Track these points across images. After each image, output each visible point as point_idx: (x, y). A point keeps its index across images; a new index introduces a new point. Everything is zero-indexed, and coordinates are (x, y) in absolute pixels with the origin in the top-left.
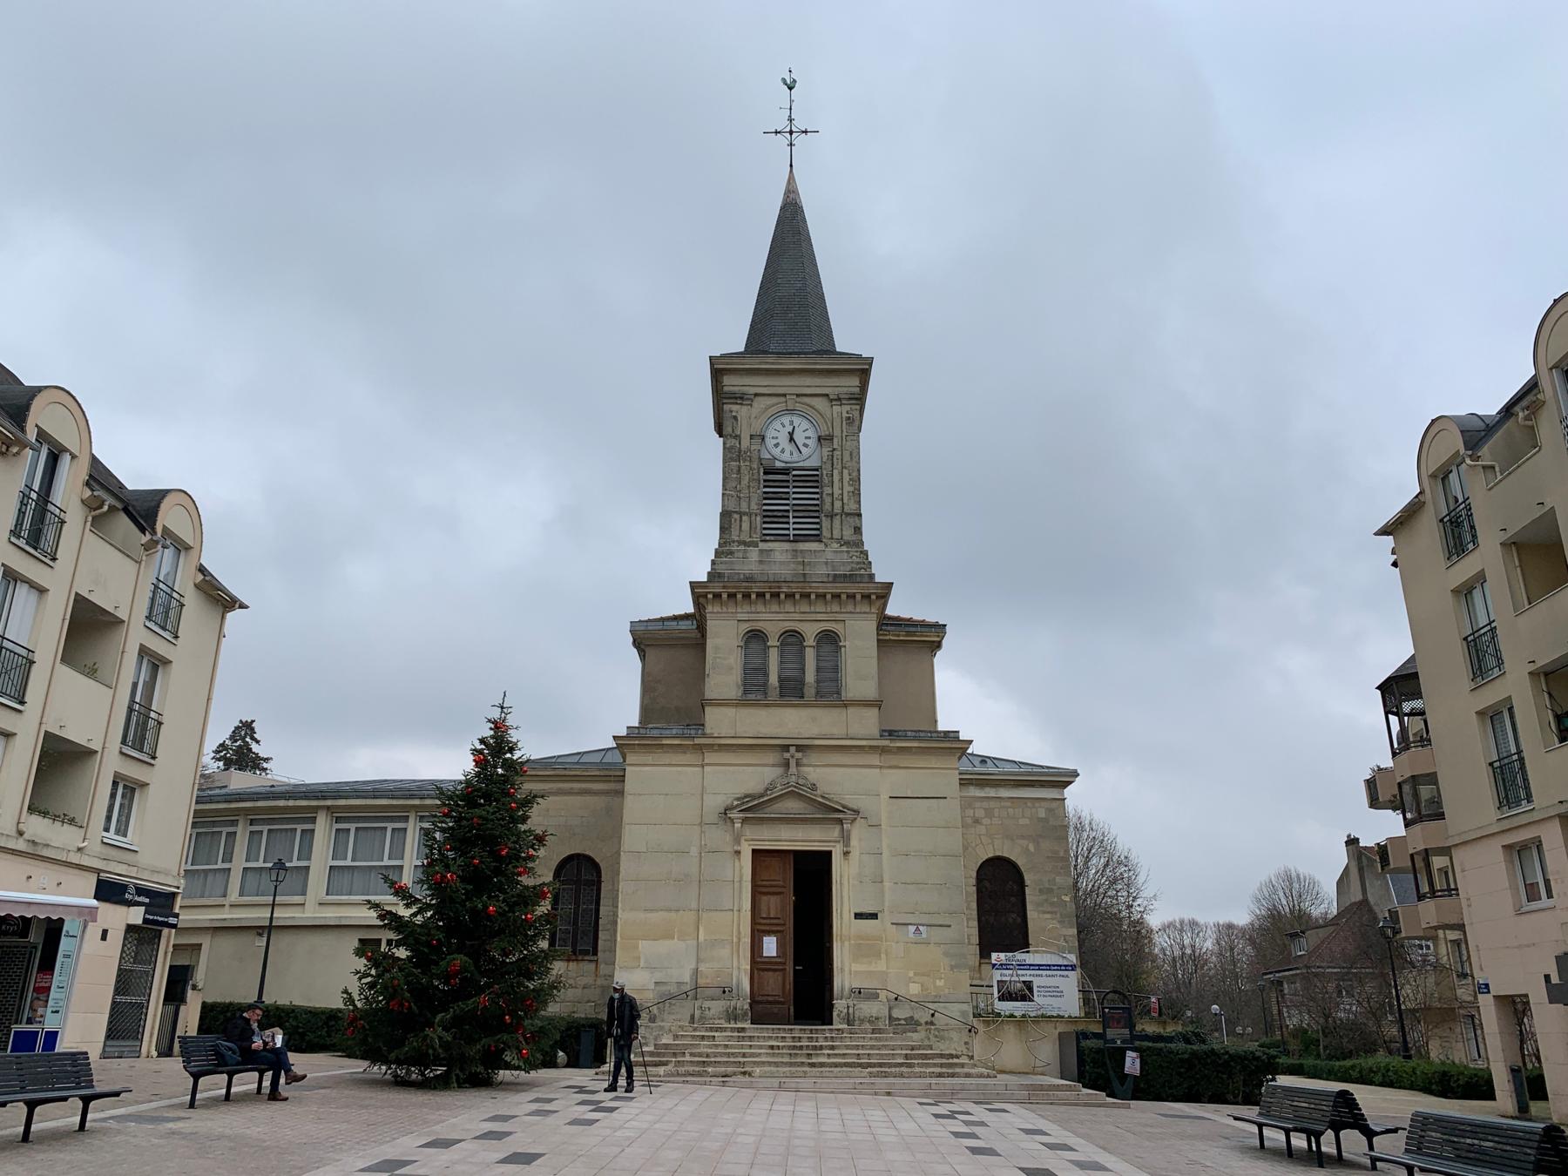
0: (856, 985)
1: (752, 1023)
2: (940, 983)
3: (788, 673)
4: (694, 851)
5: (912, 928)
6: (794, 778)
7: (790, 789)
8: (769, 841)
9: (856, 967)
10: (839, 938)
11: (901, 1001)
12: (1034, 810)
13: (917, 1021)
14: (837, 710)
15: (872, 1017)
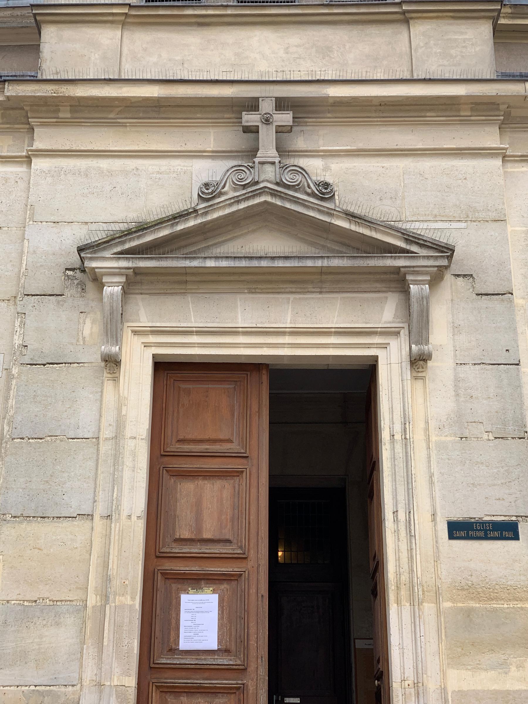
7: (262, 199)
10: (404, 593)
14: (388, 31)
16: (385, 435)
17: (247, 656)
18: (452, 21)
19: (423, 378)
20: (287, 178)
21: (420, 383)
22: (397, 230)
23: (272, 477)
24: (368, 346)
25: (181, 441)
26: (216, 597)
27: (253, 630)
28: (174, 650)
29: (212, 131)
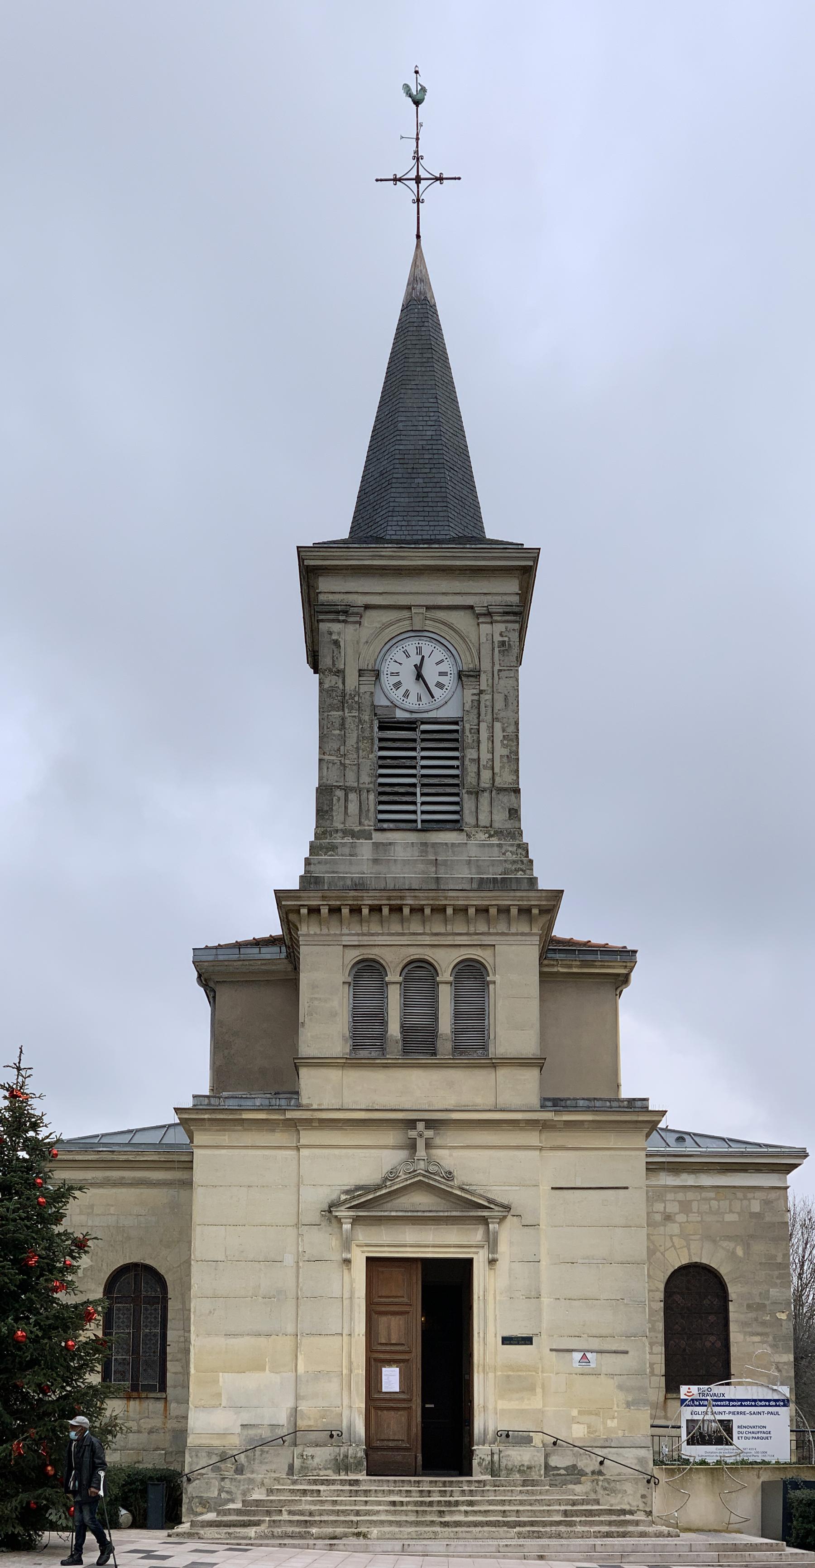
0: (504, 1426)
1: (368, 1475)
2: (611, 1424)
3: (415, 1021)
5: (577, 1356)
6: (422, 1165)
9: (502, 1405)
10: (481, 1368)
12: (745, 1202)
13: (582, 1470)
15: (523, 1465)
16: (475, 1297)
17: (412, 1395)
18: (519, 1068)
19: (494, 1269)
20: (432, 1168)
21: (493, 1271)
22: (484, 1197)
23: (422, 1282)
24: (469, 1253)
25: (380, 1297)
26: (398, 1369)
27: (414, 1383)
28: (380, 1392)
29: (392, 1132)
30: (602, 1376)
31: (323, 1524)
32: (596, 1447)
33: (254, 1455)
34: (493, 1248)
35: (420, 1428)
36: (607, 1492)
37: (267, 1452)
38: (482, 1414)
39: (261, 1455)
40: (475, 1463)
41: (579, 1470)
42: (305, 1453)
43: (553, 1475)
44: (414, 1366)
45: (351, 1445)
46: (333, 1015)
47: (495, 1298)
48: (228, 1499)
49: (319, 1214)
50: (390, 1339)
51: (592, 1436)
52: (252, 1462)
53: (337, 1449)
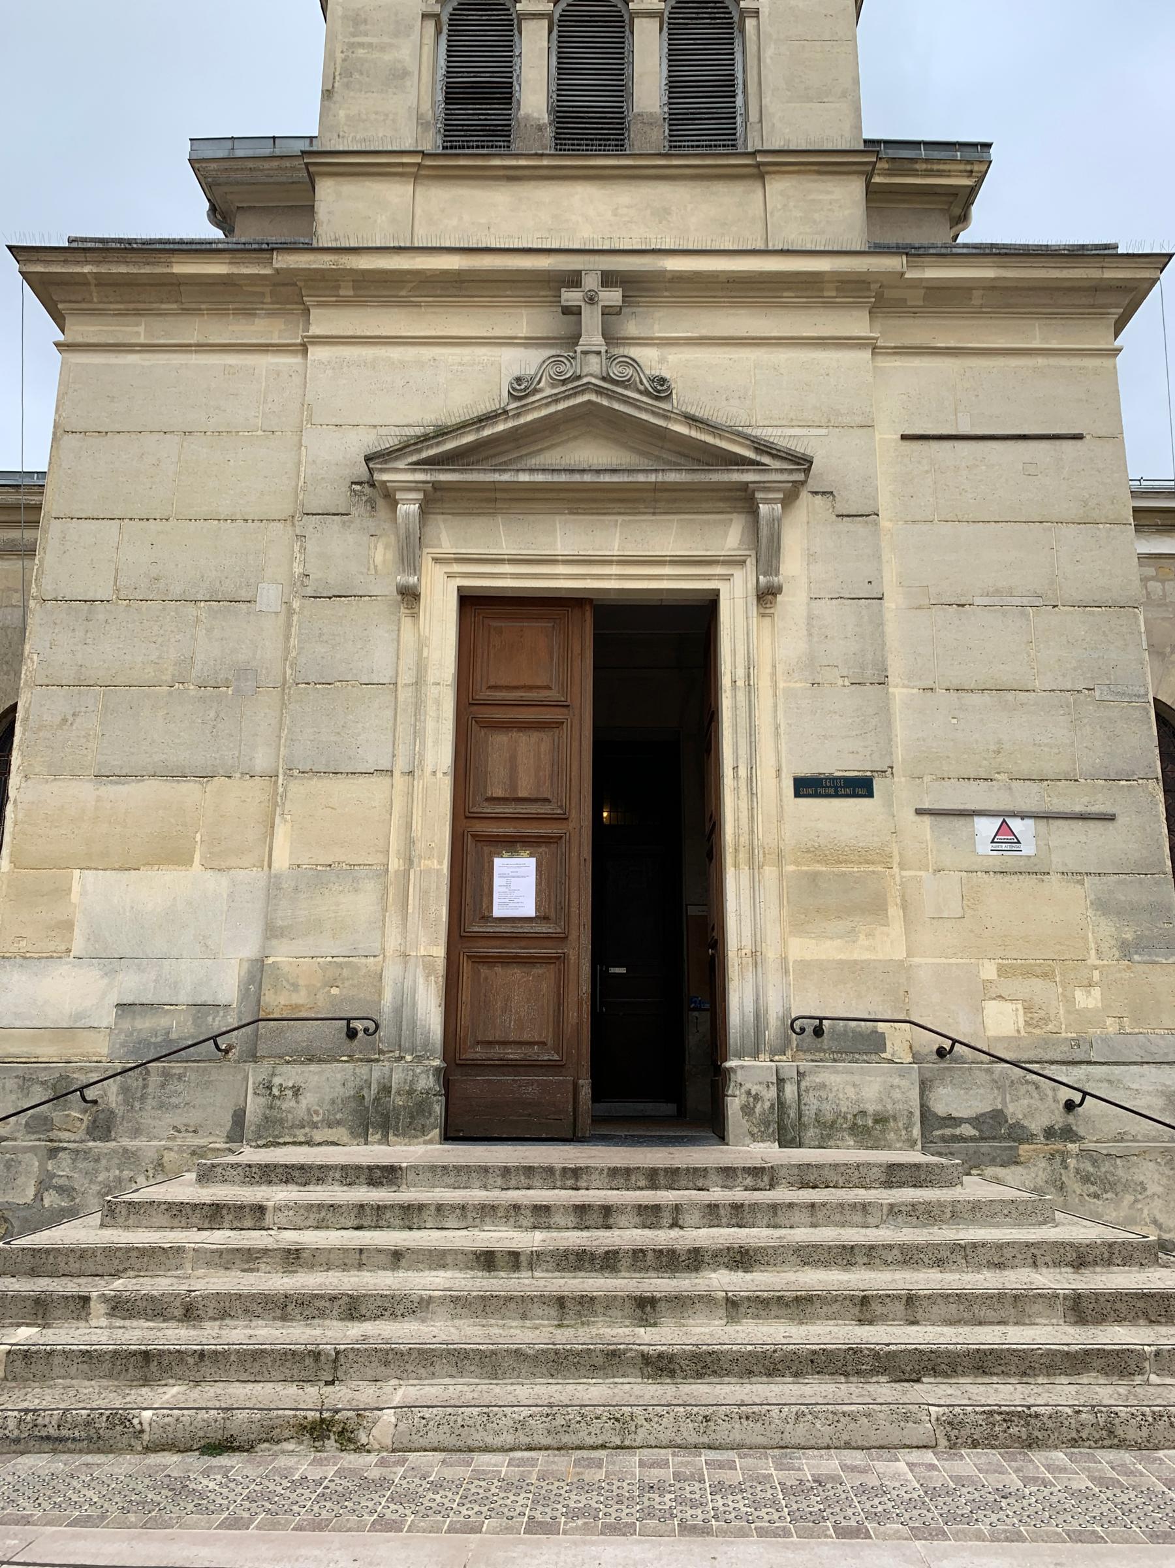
0: (807, 1004)
1: (450, 1136)
2: (1088, 1000)
3: (581, 101)
4: (270, 596)
5: (987, 827)
6: (594, 365)
8: (512, 561)
9: (801, 949)
10: (743, 856)
11: (961, 1060)
13: (1018, 1125)
15: (863, 1113)
16: (726, 681)
17: (568, 923)
19: (771, 615)
20: (615, 371)
21: (767, 620)
22: (746, 437)
24: (709, 578)
27: (574, 896)
28: (487, 917)
29: (524, 311)
30: (1054, 878)
31: (207, 1369)
32: (1052, 1063)
33: (145, 1086)
34: (769, 563)
35: (586, 1008)
36: (1093, 1189)
37: (180, 1077)
38: (749, 975)
39: (163, 1086)
40: (734, 1105)
41: (1011, 1127)
42: (277, 1081)
43: (943, 1139)
44: (574, 854)
45: (402, 1058)
46: (398, 75)
47: (775, 686)
48: (62, 1209)
49: (345, 489)
50: (514, 786)
51: (1037, 1031)
52: (137, 1105)
53: (363, 1069)
